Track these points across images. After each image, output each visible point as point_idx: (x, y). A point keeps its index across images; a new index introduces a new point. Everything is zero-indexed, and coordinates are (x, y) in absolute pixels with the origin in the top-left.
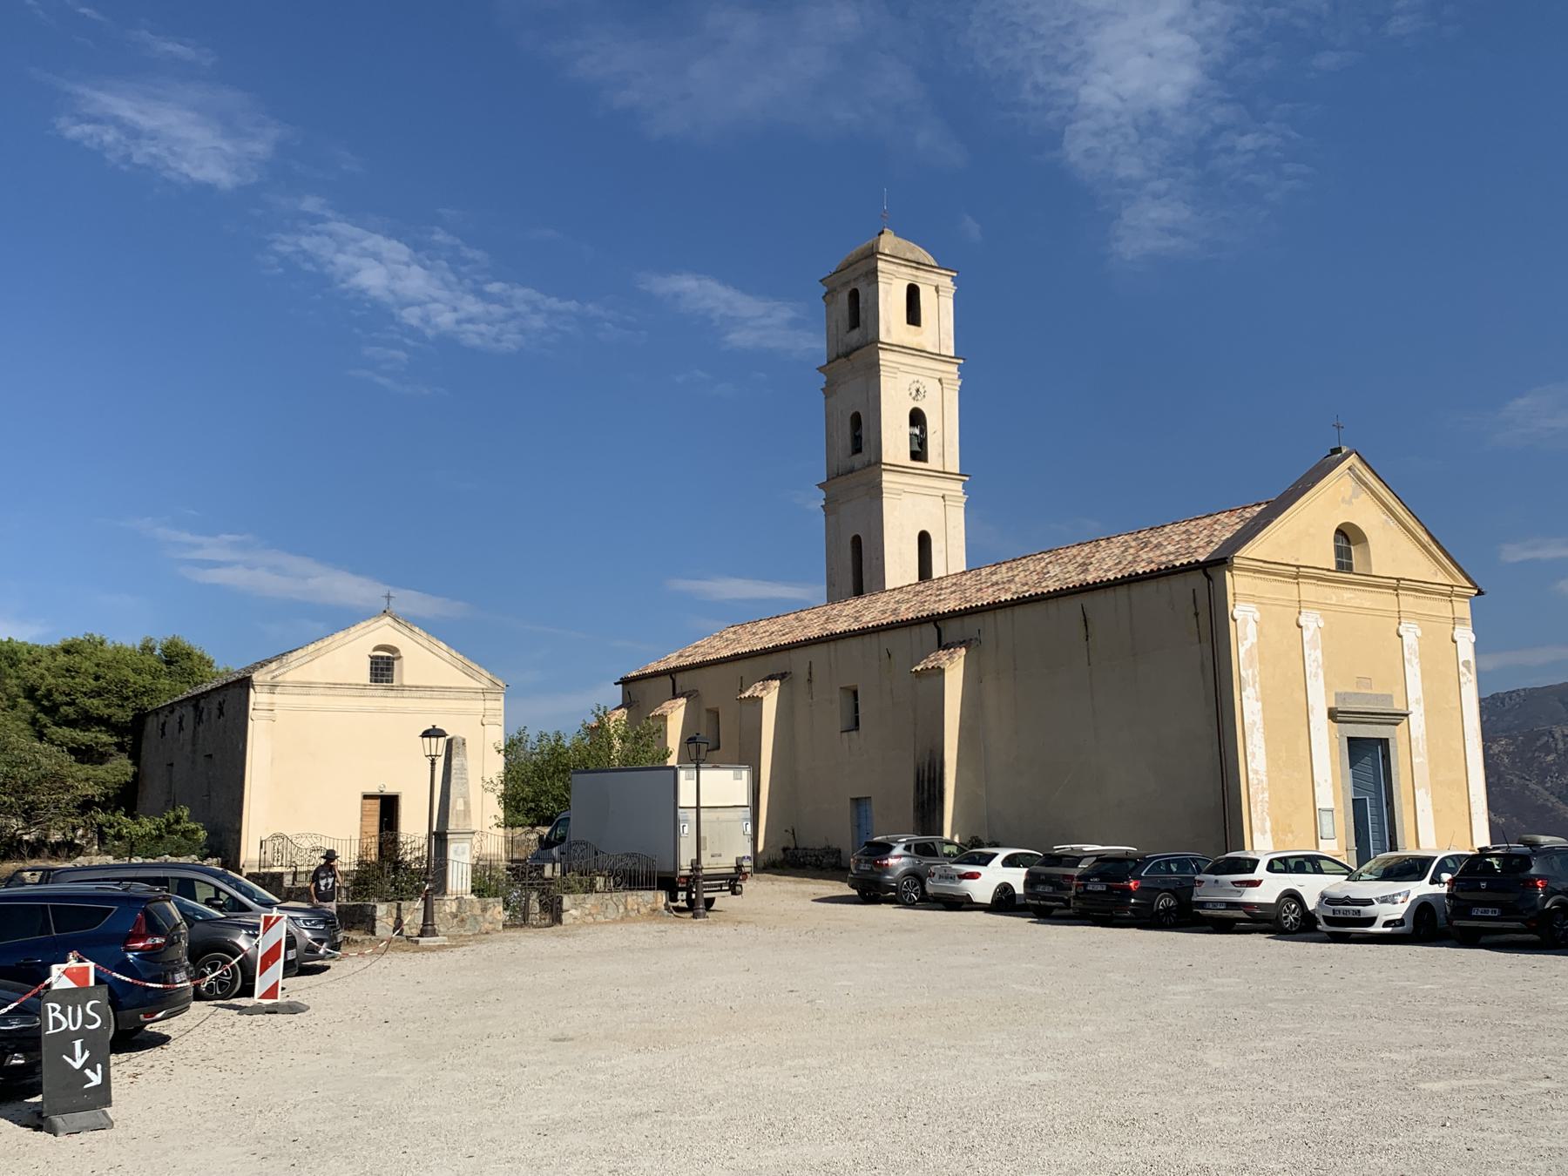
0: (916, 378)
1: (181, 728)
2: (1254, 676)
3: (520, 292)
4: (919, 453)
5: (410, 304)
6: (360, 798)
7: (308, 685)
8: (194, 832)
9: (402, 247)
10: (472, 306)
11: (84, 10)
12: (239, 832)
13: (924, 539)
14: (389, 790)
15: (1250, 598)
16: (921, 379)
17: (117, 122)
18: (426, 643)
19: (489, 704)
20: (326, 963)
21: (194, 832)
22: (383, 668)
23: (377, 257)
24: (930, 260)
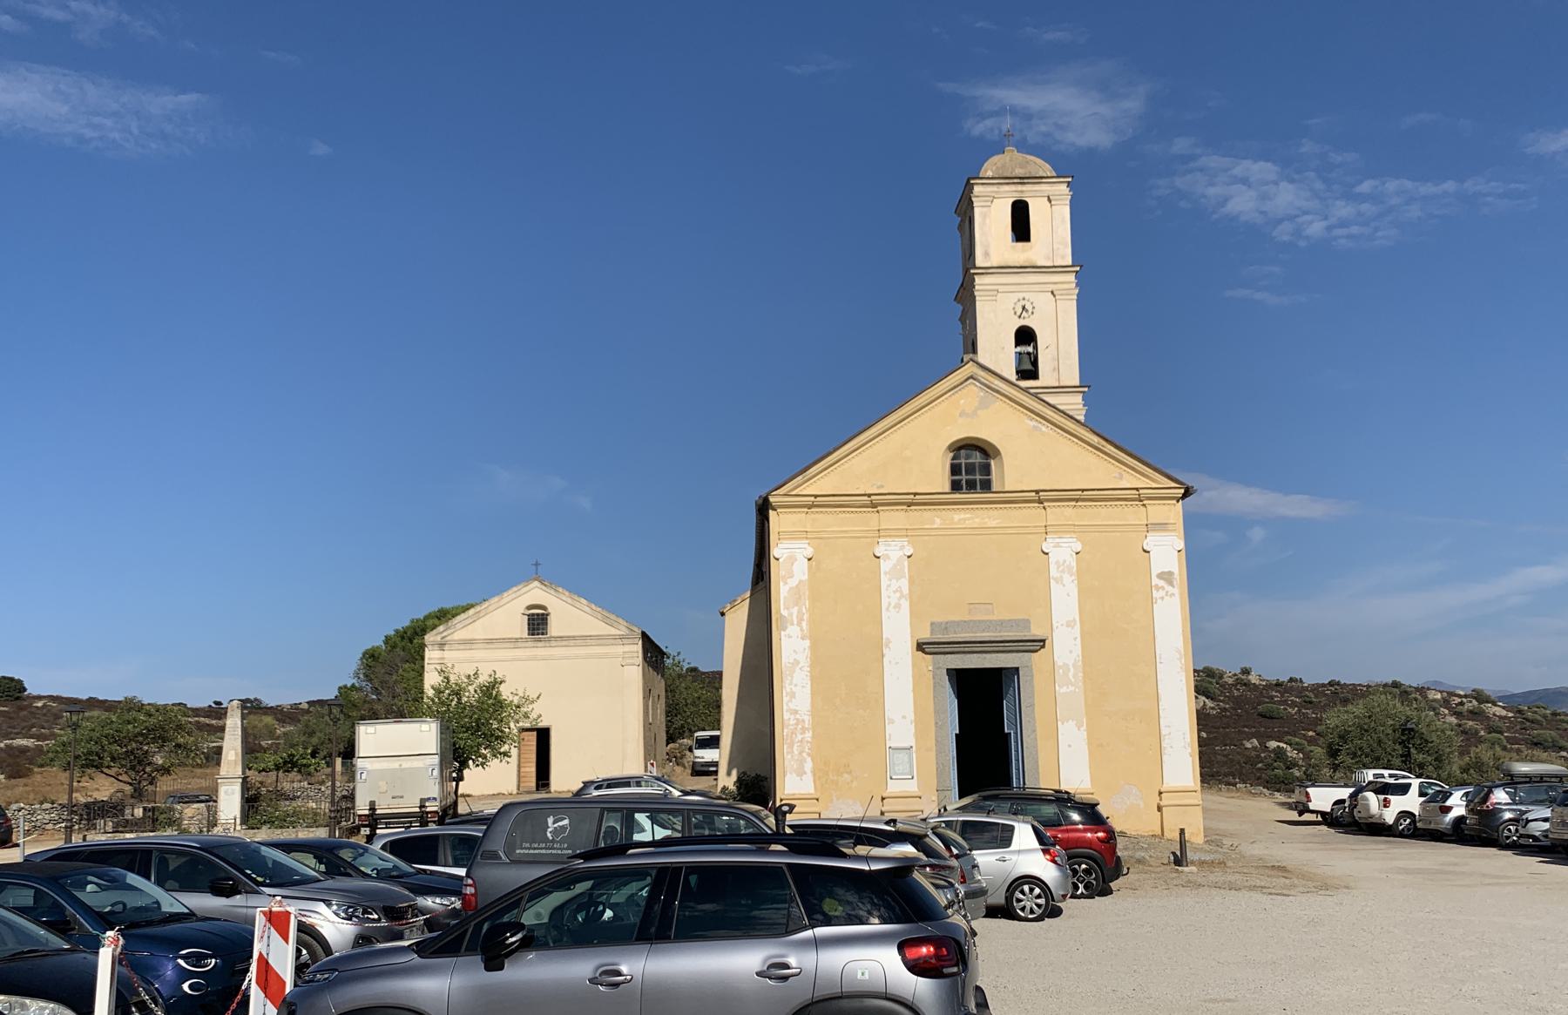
0: (1021, 296)
3: (1392, 185)
5: (1280, 221)
7: (469, 643)
9: (1269, 165)
10: (1343, 210)
11: (979, 25)
14: (542, 725)
15: (793, 536)
16: (1027, 296)
17: (1014, 111)
19: (627, 648)
20: (579, 864)
22: (538, 623)
23: (1245, 181)
24: (1046, 169)
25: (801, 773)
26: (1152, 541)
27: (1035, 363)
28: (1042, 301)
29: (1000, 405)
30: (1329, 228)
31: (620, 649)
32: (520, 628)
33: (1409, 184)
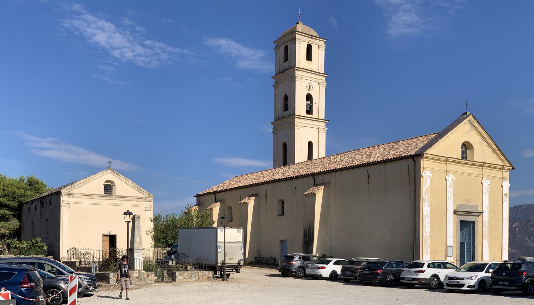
0: (309, 81)
1: (36, 209)
3: (158, 45)
5: (116, 49)
6: (102, 236)
7: (81, 195)
8: (43, 246)
10: (139, 50)
12: (59, 247)
13: (310, 144)
14: (112, 233)
16: (311, 82)
18: (124, 180)
19: (148, 203)
20: (92, 293)
21: (43, 246)
22: (108, 189)
23: (103, 29)
29: (474, 132)
30: (134, 56)
32: (102, 191)
33: (164, 46)
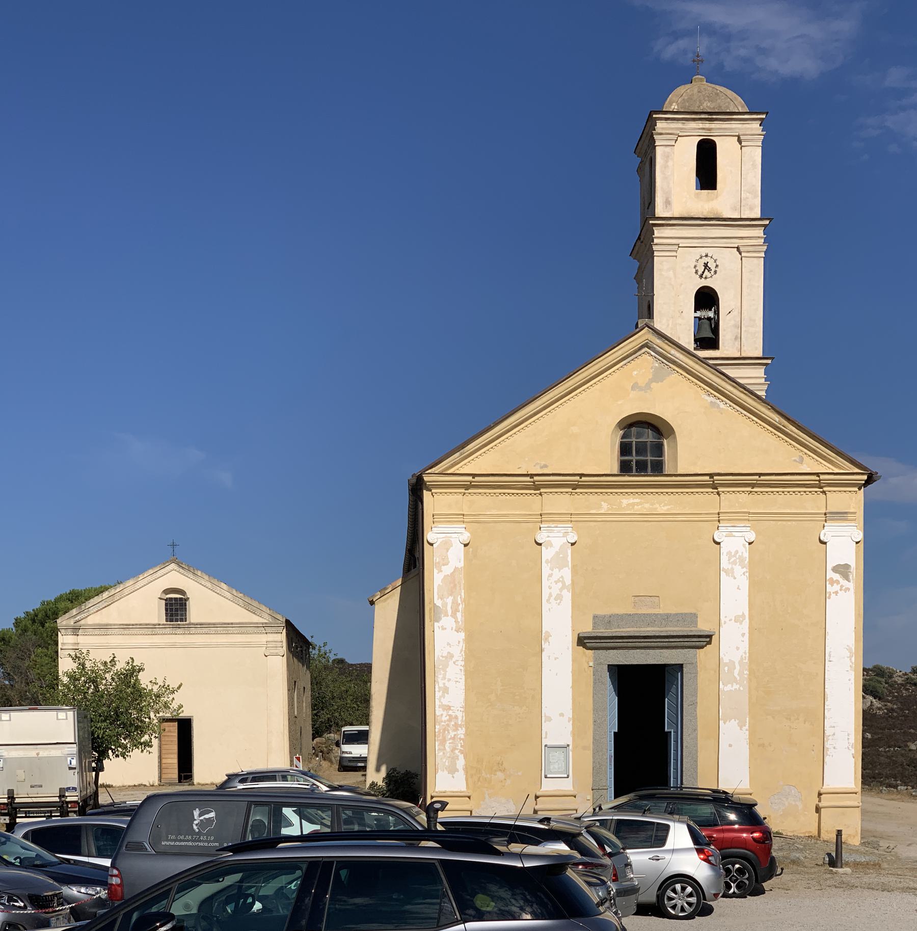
0: (703, 251)
2: (455, 602)
4: (708, 338)
7: (104, 628)
14: (184, 714)
15: (449, 518)
16: (710, 251)
18: (209, 585)
20: (229, 856)
22: (176, 608)
24: (737, 103)
25: (452, 770)
26: (830, 532)
27: (715, 330)
28: (727, 260)
31: (263, 638)
32: (156, 613)
